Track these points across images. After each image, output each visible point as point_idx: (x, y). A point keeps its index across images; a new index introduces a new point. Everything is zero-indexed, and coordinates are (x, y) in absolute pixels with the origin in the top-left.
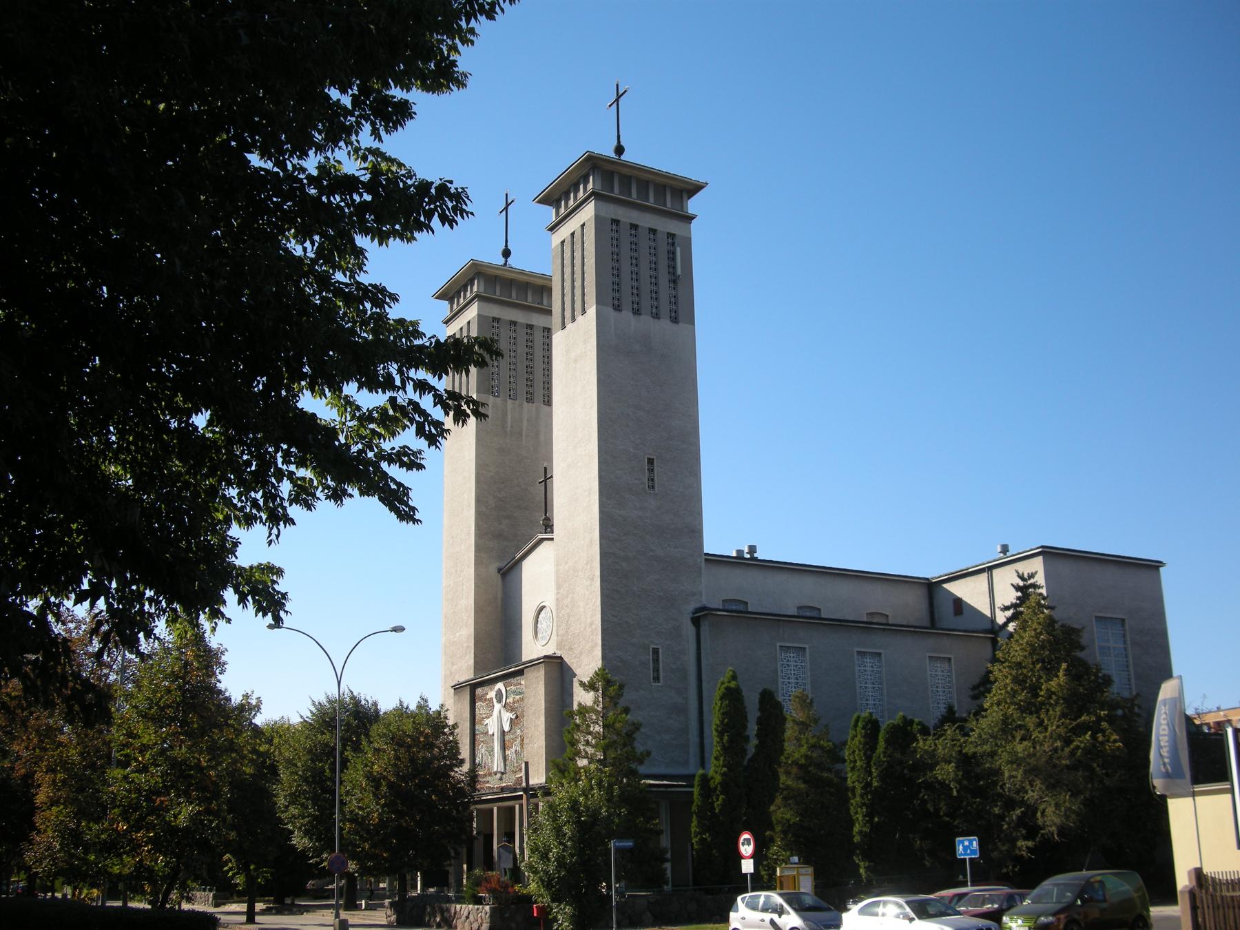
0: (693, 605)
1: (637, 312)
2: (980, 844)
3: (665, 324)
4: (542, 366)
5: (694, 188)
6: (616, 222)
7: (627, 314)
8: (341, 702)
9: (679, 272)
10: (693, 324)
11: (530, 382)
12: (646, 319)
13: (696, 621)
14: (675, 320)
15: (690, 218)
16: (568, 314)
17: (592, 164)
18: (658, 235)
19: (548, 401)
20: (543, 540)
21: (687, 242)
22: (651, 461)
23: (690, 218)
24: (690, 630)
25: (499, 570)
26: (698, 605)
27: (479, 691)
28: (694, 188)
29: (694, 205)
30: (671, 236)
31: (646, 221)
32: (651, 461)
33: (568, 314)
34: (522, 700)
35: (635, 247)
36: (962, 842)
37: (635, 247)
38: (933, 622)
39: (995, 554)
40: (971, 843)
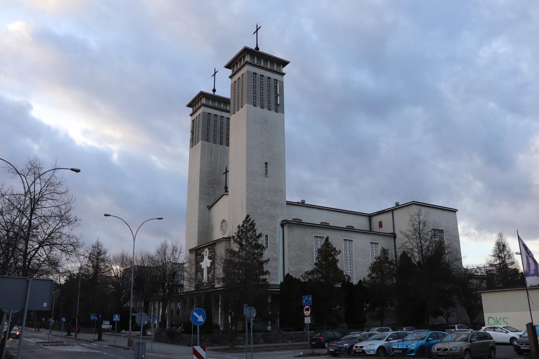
0: (280, 220)
1: (262, 107)
2: (312, 299)
3: (273, 112)
4: (226, 127)
5: (284, 63)
6: (255, 74)
7: (258, 108)
8: (165, 265)
9: (278, 92)
10: (283, 113)
11: (221, 138)
12: (266, 111)
13: (282, 225)
14: (277, 112)
15: (283, 74)
16: (236, 108)
17: (246, 51)
18: (271, 80)
19: (228, 145)
20: (223, 195)
21: (282, 83)
22: (266, 163)
23: (283, 74)
24: (281, 229)
25: (208, 207)
26: (283, 219)
27: (199, 251)
28: (284, 63)
29: (284, 70)
30: (276, 80)
31: (267, 74)
32: (266, 163)
33: (236, 108)
34: (215, 255)
35: (262, 83)
36: (305, 298)
37: (262, 83)
38: (371, 230)
39: (392, 205)
40: (308, 298)
